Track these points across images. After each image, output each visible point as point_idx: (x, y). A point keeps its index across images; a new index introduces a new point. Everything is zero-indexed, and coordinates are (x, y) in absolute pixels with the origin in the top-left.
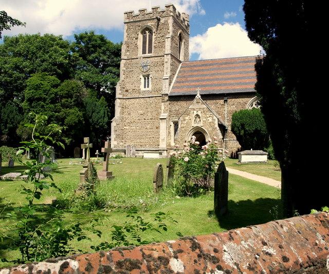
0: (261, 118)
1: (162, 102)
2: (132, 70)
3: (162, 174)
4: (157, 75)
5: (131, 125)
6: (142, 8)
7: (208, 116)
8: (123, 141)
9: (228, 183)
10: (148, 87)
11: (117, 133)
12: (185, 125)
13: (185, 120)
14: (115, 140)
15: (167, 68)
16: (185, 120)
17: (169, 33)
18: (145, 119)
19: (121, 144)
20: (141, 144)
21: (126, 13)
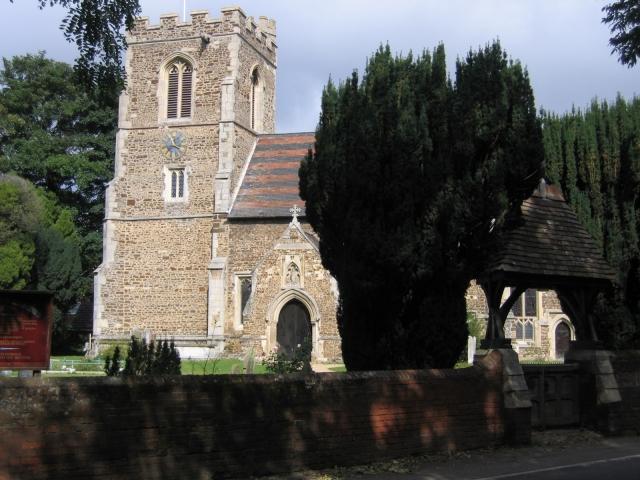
4: (202, 168)
5: (142, 282)
10: (181, 195)
13: (265, 275)
14: (103, 317)
16: (265, 275)
17: (230, 72)
19: (118, 325)
20: (165, 327)
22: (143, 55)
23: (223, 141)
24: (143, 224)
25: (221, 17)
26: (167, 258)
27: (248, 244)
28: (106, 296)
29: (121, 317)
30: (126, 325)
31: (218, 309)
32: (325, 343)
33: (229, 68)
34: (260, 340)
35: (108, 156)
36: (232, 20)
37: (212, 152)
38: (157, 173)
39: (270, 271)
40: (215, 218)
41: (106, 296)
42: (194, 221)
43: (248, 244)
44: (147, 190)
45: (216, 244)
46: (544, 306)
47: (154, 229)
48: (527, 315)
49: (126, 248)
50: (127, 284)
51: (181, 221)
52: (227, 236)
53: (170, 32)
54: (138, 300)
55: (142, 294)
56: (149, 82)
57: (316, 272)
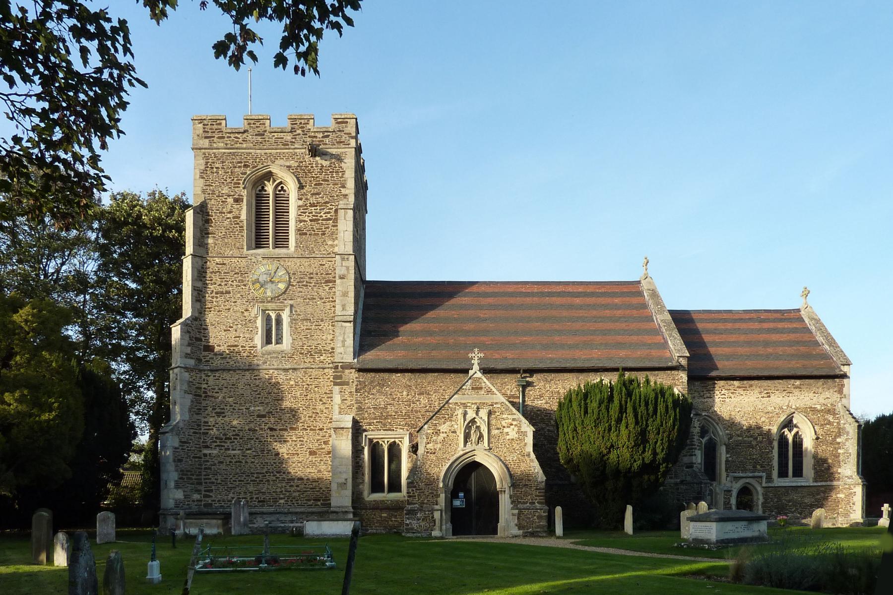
0: (67, 574)
1: (336, 384)
2: (225, 289)
3: (822, 359)
4: (309, 310)
5: (228, 444)
6: (257, 113)
7: (503, 423)
8: (202, 488)
9: (562, 549)
10: (279, 341)
11: (183, 466)
12: (439, 446)
13: (437, 433)
14: (177, 487)
15: (345, 294)
16: (437, 433)
17: (345, 196)
18: (271, 429)
19: (196, 496)
20: (262, 497)
21: (201, 121)
22: (220, 166)
23: (341, 278)
24: (226, 375)
25: (331, 125)
26: (264, 416)
27: (381, 400)
28: (180, 461)
29: (199, 487)
30: (206, 496)
31: (344, 476)
32: (519, 514)
33: (344, 191)
34: (433, 511)
35: (299, 230)
36: (347, 130)
37: (324, 290)
38: (246, 314)
39: (444, 428)
40: (336, 367)
41: (180, 461)
42: (300, 374)
43: (381, 400)
44: (233, 334)
45: (337, 399)
46: (726, 470)
47: (244, 380)
48: (794, 476)
49: (204, 403)
50: (207, 447)
51: (281, 372)
52: (353, 390)
53: (259, 138)
54: (223, 467)
55: (228, 459)
56: (230, 200)
57: (506, 430)
